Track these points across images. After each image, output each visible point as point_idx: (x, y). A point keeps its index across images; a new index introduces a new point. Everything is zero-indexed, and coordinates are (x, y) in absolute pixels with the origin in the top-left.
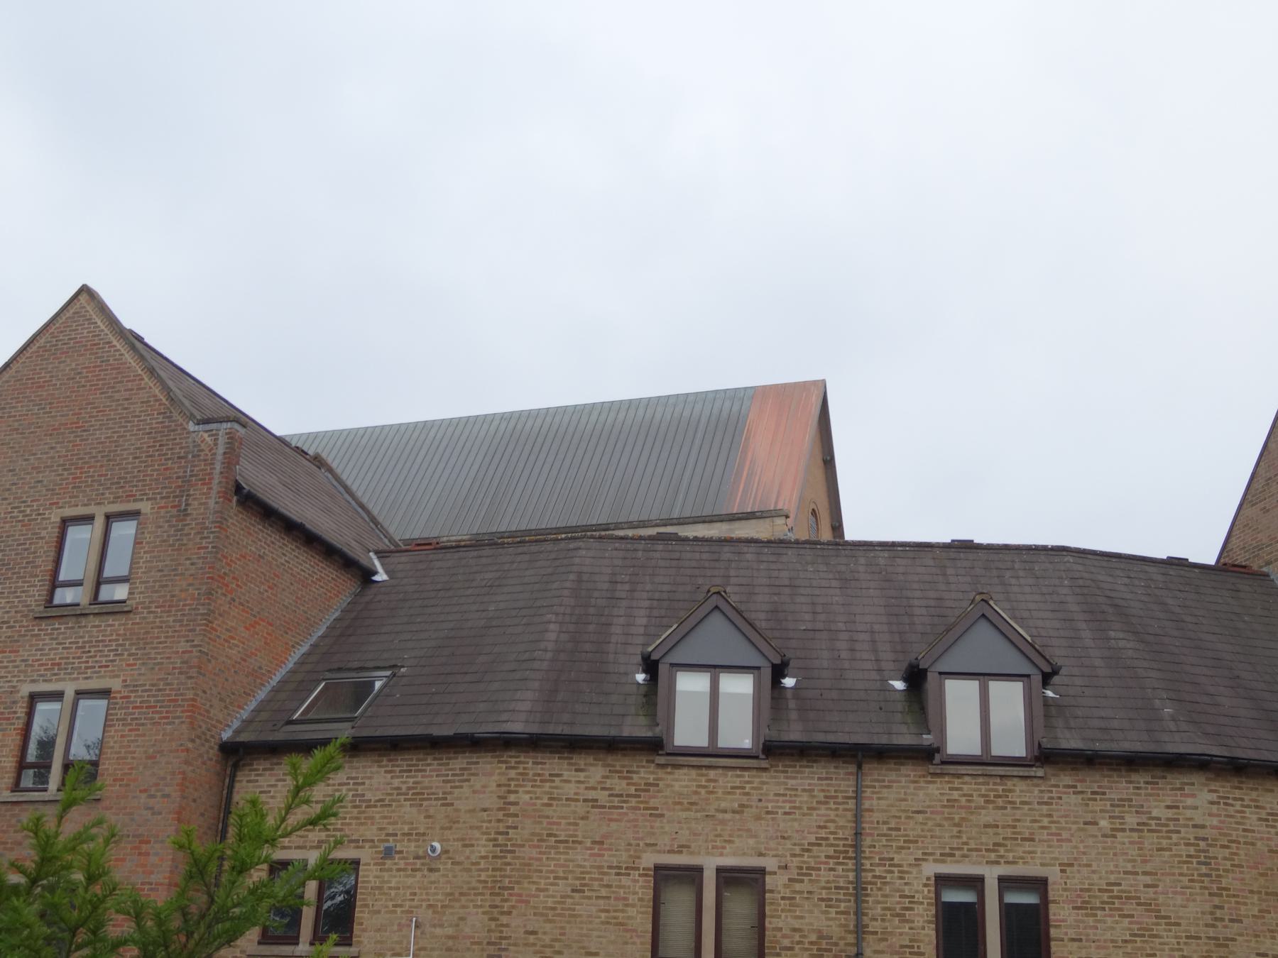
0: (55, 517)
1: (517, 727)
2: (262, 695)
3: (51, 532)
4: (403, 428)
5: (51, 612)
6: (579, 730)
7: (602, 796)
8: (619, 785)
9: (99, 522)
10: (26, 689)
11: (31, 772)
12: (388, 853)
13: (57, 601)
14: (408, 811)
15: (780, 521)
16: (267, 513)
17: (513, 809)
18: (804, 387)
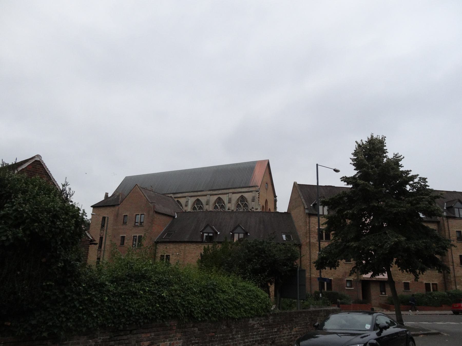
0: (135, 214)
1: (186, 240)
2: (160, 235)
3: (134, 216)
4: (199, 169)
5: (135, 226)
6: (193, 240)
7: (195, 248)
8: (197, 247)
9: (140, 215)
10: (133, 235)
11: (134, 245)
12: (173, 254)
13: (136, 224)
14: (175, 249)
15: (257, 187)
16: (159, 213)
17: (185, 250)
18: (265, 161)
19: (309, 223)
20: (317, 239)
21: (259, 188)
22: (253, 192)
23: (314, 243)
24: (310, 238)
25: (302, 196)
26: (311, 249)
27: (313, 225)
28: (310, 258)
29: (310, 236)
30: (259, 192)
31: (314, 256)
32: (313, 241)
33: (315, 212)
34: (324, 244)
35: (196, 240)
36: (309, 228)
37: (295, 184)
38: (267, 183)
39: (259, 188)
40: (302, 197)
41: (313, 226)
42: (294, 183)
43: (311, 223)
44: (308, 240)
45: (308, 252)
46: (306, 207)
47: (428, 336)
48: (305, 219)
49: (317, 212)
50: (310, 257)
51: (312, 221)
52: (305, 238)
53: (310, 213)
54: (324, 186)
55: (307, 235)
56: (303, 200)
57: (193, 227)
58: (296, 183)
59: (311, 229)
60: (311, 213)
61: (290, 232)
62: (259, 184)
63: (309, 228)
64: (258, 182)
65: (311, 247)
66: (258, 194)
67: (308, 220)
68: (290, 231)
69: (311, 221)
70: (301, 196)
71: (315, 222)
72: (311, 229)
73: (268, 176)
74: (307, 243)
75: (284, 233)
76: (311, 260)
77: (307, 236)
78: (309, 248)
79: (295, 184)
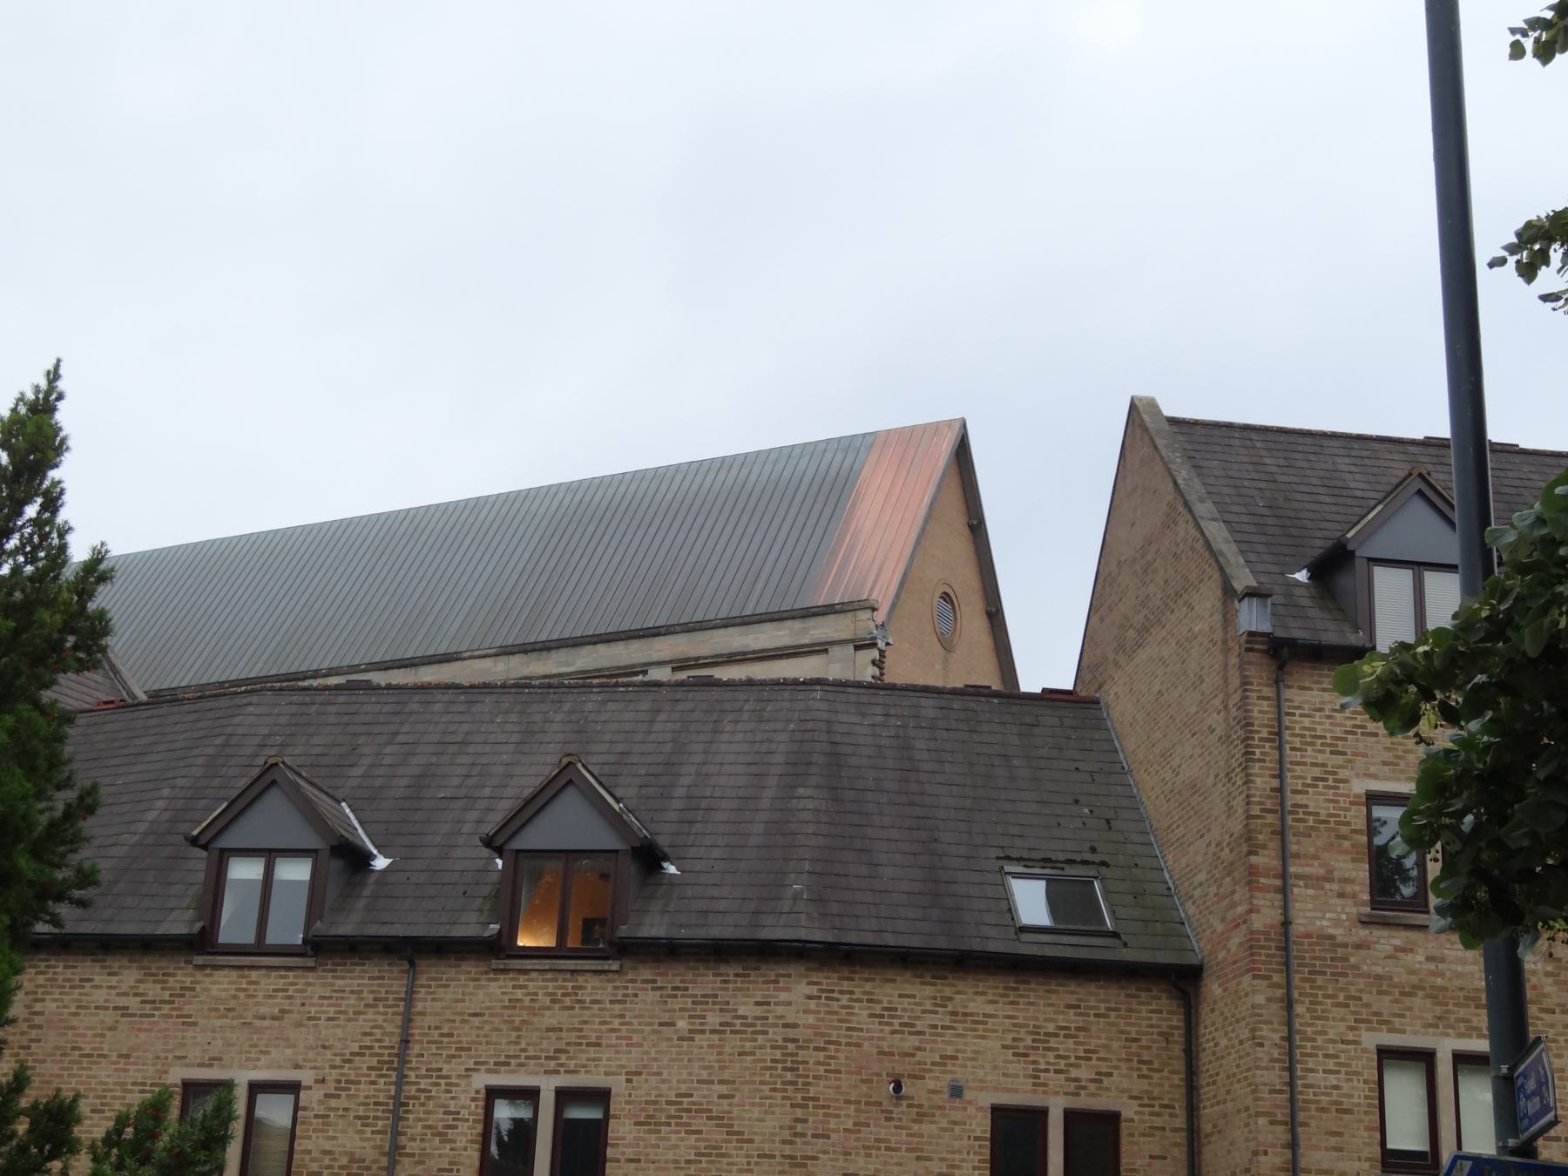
4: (451, 508)
7: (133, 1003)
8: (152, 990)
15: (864, 615)
17: (37, 1020)
18: (935, 428)
19: (1278, 734)
20: (1366, 897)
21: (879, 622)
22: (835, 651)
23: (1332, 937)
24: (1284, 891)
25: (1202, 501)
26: (1299, 1009)
27: (1320, 759)
28: (1292, 1100)
29: (1292, 869)
30: (882, 653)
31: (1333, 1080)
32: (1325, 924)
33: (1332, 632)
34: (1430, 959)
35: (148, 930)
36: (1275, 783)
37: (1140, 416)
38: (946, 597)
39: (880, 616)
40: (1204, 509)
41: (1317, 772)
42: (1133, 407)
43: (1297, 742)
44: (1267, 915)
45: (1273, 1034)
46: (1243, 579)
47: (235, 1107)
48: (1236, 698)
49: (1356, 629)
50: (1291, 1084)
51: (1307, 722)
52: (1241, 893)
53: (1280, 633)
54: (1413, 442)
55: (1253, 859)
56: (1217, 532)
57: (151, 815)
58: (1152, 405)
59: (1299, 799)
60: (1299, 633)
61: (1088, 857)
62: (883, 595)
63: (1280, 790)
64: (875, 582)
65: (1296, 977)
66: (874, 662)
67: (1261, 712)
68: (1093, 850)
69: (1298, 723)
70: (1191, 498)
71: (1338, 732)
72: (1299, 799)
73: (961, 545)
74: (1251, 945)
75: (1032, 864)
76: (1301, 1116)
77: (1253, 872)
78: (1280, 993)
79: (1140, 416)
